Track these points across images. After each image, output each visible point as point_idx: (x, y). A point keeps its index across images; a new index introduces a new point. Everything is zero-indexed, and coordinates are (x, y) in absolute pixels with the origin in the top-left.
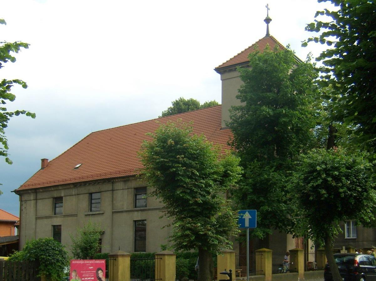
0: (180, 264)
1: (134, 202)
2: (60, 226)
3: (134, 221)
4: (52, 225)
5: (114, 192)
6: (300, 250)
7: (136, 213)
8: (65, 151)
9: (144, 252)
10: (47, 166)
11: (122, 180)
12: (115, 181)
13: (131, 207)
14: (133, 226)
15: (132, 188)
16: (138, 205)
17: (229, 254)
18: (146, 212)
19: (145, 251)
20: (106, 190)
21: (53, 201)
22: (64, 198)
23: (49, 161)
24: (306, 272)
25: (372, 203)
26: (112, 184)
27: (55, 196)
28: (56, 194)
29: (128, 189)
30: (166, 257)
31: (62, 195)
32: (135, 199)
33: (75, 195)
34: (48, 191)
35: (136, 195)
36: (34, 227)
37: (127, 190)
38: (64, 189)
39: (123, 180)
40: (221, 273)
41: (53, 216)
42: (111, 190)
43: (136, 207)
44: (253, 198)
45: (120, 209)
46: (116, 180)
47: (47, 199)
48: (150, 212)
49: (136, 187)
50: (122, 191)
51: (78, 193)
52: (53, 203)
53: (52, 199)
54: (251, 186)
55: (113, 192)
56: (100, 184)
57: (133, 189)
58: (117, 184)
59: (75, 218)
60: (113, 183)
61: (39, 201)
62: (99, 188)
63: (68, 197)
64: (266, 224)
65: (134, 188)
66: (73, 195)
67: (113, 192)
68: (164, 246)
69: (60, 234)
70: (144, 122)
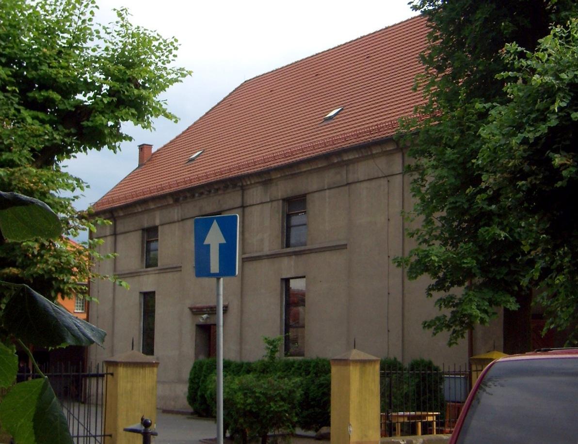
0: (271, 392)
1: (282, 233)
2: (154, 293)
3: (282, 279)
4: (140, 293)
5: (248, 210)
6: (127, 364)
7: (285, 261)
8: (190, 125)
9: (300, 358)
10: (149, 161)
11: (257, 181)
12: (245, 184)
13: (277, 248)
14: (281, 294)
15: (278, 200)
16: (293, 241)
17: (358, 368)
18: (304, 257)
19: (303, 355)
20: (231, 207)
21: (143, 237)
22: (160, 228)
23: (154, 150)
24: (388, 439)
25: (16, 148)
26: (240, 193)
27: (146, 225)
28: (146, 221)
29: (272, 201)
30: (121, 371)
31: (157, 222)
32: (287, 225)
33: (178, 221)
34: (130, 214)
35: (288, 217)
36: (111, 296)
37: (270, 204)
38: (158, 207)
39: (260, 180)
40: (126, 430)
41: (141, 272)
42: (239, 206)
43: (288, 245)
44: (458, 204)
45: (256, 252)
46: (246, 182)
47: (133, 233)
48: (313, 255)
49: (285, 197)
50: (260, 206)
51: (184, 218)
52: (143, 241)
53: (140, 232)
54: (454, 169)
55: (243, 212)
56: (220, 192)
57: (281, 201)
58: (251, 191)
59: (176, 275)
60: (243, 189)
61: (120, 238)
62: (219, 201)
63: (167, 226)
64: (498, 277)
65: (284, 200)
66: (174, 222)
67: (243, 212)
68: (273, 341)
69: (153, 311)
70: (341, 45)
